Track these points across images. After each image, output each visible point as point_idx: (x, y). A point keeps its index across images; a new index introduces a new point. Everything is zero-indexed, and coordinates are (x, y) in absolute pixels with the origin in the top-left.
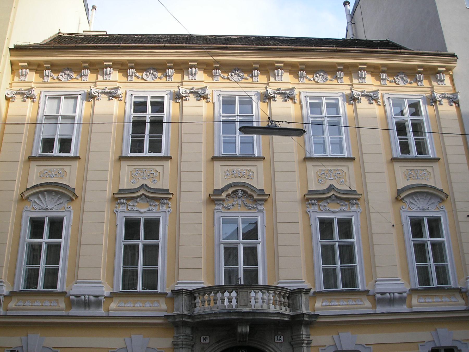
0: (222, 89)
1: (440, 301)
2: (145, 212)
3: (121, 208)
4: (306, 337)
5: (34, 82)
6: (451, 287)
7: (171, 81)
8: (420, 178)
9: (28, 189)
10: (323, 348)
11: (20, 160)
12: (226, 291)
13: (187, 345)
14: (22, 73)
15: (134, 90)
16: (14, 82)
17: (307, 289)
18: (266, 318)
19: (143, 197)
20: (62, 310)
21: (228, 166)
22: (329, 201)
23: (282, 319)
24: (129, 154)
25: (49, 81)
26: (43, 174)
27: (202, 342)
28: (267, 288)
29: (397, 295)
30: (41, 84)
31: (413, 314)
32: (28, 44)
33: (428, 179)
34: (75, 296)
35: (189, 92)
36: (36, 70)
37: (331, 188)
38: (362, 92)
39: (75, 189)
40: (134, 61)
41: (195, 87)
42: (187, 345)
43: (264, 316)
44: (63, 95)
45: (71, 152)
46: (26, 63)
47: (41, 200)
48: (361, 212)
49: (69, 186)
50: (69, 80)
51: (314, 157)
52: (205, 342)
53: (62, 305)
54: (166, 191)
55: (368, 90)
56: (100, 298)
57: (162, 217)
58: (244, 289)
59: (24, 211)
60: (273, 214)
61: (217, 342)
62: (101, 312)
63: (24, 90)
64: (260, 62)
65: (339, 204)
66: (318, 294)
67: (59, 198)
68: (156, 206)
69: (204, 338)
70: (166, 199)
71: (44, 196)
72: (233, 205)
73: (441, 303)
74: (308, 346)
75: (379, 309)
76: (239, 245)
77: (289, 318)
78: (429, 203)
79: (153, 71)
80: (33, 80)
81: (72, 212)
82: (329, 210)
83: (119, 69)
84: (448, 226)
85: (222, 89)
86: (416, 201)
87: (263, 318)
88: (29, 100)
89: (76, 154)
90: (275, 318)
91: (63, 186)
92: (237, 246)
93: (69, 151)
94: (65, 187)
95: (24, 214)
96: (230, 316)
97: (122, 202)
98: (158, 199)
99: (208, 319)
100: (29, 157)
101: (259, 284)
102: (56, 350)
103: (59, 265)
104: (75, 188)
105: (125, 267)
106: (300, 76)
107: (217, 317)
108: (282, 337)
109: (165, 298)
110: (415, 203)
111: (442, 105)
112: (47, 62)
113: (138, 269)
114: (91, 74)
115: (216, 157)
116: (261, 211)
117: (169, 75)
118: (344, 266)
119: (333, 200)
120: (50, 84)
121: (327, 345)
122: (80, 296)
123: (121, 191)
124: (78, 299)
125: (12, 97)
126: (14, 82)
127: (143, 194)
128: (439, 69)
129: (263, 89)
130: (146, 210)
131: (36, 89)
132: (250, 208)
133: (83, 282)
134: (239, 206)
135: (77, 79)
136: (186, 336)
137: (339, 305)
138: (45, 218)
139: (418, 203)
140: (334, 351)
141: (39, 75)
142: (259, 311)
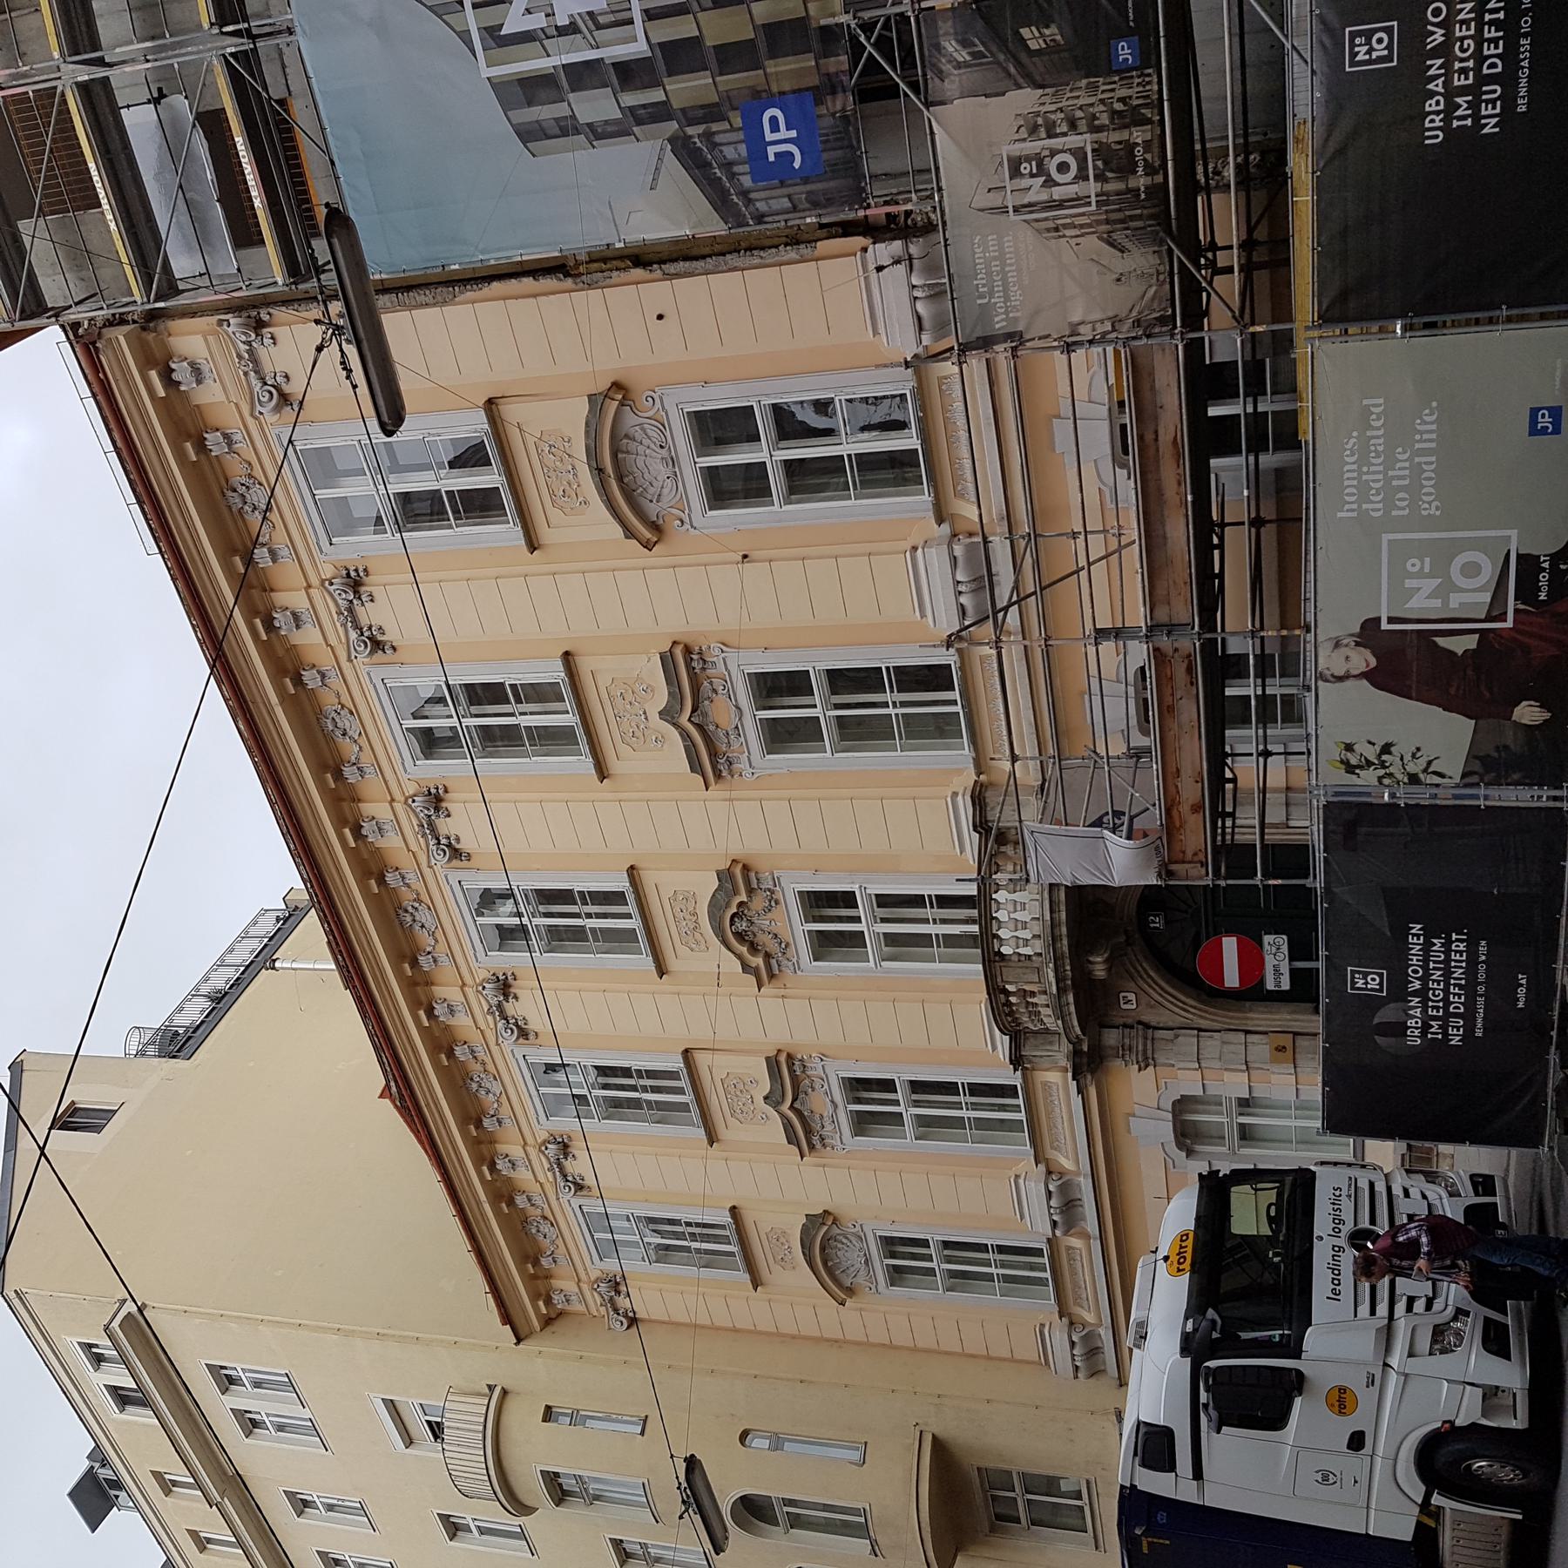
19: (797, 1105)
24: (584, 746)
27: (1134, 1007)
32: (489, 1295)
37: (668, 714)
44: (592, 1236)
46: (537, 1305)
52: (1134, 1002)
54: (667, 660)
76: (868, 891)
85: (312, 540)
92: (881, 936)
96: (1070, 1014)
99: (1065, 942)
101: (975, 893)
107: (1068, 1004)
119: (705, 715)
122: (961, 605)
124: (926, 324)
138: (700, 468)
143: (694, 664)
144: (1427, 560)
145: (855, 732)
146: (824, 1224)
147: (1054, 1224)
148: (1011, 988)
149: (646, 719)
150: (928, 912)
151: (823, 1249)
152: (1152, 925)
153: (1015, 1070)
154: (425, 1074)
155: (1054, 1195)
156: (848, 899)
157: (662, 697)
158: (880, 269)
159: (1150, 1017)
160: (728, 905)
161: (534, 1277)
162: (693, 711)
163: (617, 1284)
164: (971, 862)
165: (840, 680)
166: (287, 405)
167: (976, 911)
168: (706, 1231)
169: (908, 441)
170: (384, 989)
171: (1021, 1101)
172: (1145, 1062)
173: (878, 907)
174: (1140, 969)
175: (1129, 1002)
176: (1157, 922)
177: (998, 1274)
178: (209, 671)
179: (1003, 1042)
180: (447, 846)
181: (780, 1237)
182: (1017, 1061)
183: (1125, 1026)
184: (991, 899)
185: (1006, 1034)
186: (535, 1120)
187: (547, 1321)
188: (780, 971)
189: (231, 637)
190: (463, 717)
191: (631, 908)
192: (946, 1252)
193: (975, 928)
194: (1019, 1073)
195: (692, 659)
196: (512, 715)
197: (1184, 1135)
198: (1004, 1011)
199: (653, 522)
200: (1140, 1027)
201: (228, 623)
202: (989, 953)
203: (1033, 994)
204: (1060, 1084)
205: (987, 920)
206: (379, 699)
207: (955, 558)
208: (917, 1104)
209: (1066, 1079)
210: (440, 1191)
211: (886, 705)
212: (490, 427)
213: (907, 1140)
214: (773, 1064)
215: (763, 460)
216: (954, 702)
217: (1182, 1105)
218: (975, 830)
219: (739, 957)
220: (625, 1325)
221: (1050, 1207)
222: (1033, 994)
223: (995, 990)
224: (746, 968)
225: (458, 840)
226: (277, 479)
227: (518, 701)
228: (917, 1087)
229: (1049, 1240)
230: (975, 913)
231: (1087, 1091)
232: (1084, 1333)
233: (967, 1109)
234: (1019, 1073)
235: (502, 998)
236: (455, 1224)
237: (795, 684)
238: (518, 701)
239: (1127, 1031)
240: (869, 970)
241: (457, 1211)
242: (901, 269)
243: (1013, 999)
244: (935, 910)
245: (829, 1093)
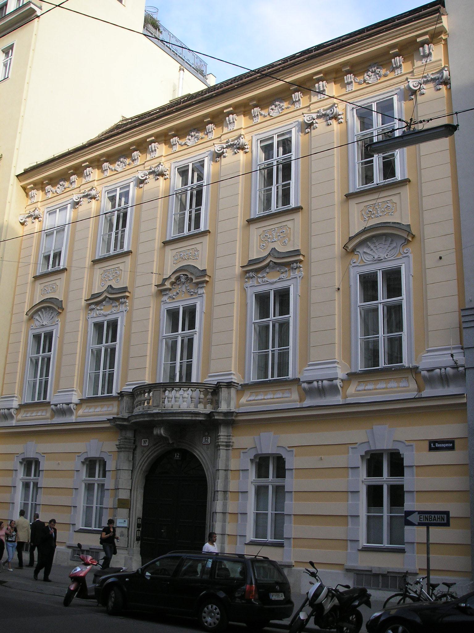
0: (178, 160)
1: (383, 387)
2: (108, 314)
3: (251, 283)
4: (227, 438)
5: (243, 127)
6: (403, 366)
7: (299, 108)
8: (381, 214)
9: (351, 239)
10: (245, 451)
11: (238, 227)
12: (189, 389)
13: (125, 448)
14: (229, 120)
15: (109, 185)
16: (312, 104)
17: (228, 382)
18: (174, 418)
19: (107, 299)
20: (295, 401)
21: (44, 284)
22: (267, 270)
23: (194, 418)
24: (262, 214)
25: (259, 121)
26: (44, 291)
28: (179, 385)
29: (325, 382)
30: (45, 201)
31: (353, 406)
33: (393, 213)
34: (307, 383)
35: (147, 173)
36: (244, 112)
38: (318, 112)
39: (410, 226)
40: (135, 142)
41: (152, 166)
42: (125, 448)
43: (172, 416)
44: (57, 208)
45: (396, 176)
47: (41, 317)
48: (302, 278)
49: (58, 299)
50: (281, 113)
51: (257, 218)
53: (295, 396)
54: (297, 253)
55: (325, 107)
56: (334, 381)
57: (120, 317)
58: (156, 388)
59: (351, 266)
60: (306, 279)
61: (154, 445)
62: (338, 400)
63: (88, 191)
64: (209, 114)
65: (279, 271)
66: (246, 387)
67: (52, 313)
68: (116, 306)
69: (144, 441)
70: (296, 262)
71: (42, 313)
72: (178, 294)
73: (399, 389)
74: (227, 448)
75: (308, 403)
77: (204, 417)
78: (390, 248)
79: (123, 159)
80: (243, 127)
81: (411, 256)
82: (267, 281)
83: (335, 79)
84: (298, 297)
85: (178, 160)
86: (374, 252)
87: (171, 418)
88: (241, 152)
89: (298, 205)
90: (185, 418)
91: (391, 225)
93: (394, 175)
94: (396, 226)
95: (90, 320)
96: (144, 417)
97: (251, 275)
98: (117, 299)
100: (346, 194)
101: (192, 382)
102: (411, 443)
103: (289, 346)
104: (409, 225)
105: (281, 350)
106: (253, 115)
108: (209, 438)
109: (118, 401)
110: (370, 252)
111: (424, 94)
112: (69, 168)
113: (268, 354)
114: (79, 178)
115: (351, 193)
116: (201, 295)
117: (254, 115)
118: (283, 349)
119: (273, 268)
120: (51, 199)
121: (249, 447)
122: (313, 382)
123: (252, 262)
125: (25, 222)
126: (312, 104)
127: (106, 297)
128: (419, 40)
129: (301, 116)
130: (109, 312)
131: (165, 163)
132: (192, 293)
133: (332, 362)
134: (183, 293)
135: (68, 187)
136: (126, 439)
137: (264, 399)
139: (374, 252)
140: (256, 454)
141: (248, 116)
142: (167, 412)
143: (295, 265)
144: (36, 552)
145: (263, 331)
146: (58, 308)
147: (56, 405)
148: (151, 394)
149: (273, 242)
150: (185, 360)
151: (49, 307)
152: (176, 454)
153: (118, 393)
154: (126, 139)
155: (330, 383)
156: (192, 326)
157: (281, 249)
158: (452, 355)
159: (138, 451)
160: (192, 274)
161: (42, 183)
162: (275, 263)
163: (38, 218)
164: (205, 380)
165: (284, 327)
166: (412, 93)
167: (185, 381)
168: (119, 241)
169: (382, 363)
170: (153, 126)
171: (106, 395)
172: (120, 448)
173: (188, 339)
174: (158, 448)
175: (145, 443)
176: (177, 456)
177: (37, 380)
178: (252, 70)
179: (129, 389)
180: (223, 152)
181: (54, 291)
182: (121, 395)
183: (135, 440)
184: (189, 388)
185: (133, 390)
186: (106, 185)
187: (24, 188)
188: (113, 307)
189: (273, 80)
190: (377, 131)
191: (193, 231)
192: (46, 359)
193: (177, 380)
194: (117, 395)
195: (297, 263)
196: (277, 183)
197: (90, 461)
198: (142, 390)
199: (355, 249)
200: (134, 447)
201: (278, 79)
202: (166, 385)
203: (148, 403)
204: (112, 412)
205: (180, 385)
206: (284, 126)
207: (333, 380)
208: (106, 350)
209: (113, 414)
210: (79, 144)
211: (273, 347)
212: (399, 181)
213: (31, 353)
214: (125, 289)
215: (270, 317)
216: (272, 376)
217: (103, 463)
218: (218, 382)
219: (170, 277)
220: (21, 221)
221: (63, 404)
222: (148, 403)
223: (151, 387)
224: (165, 280)
225: (225, 157)
226: (341, 100)
227: (283, 186)
228: (113, 350)
229: (49, 402)
230: (184, 380)
231: (108, 423)
232: (13, 414)
233: (103, 372)
234: (117, 395)
235: (157, 173)
236: (64, 150)
237: (284, 308)
238: (283, 186)
239: (133, 441)
240: (163, 334)
241: (85, 145)
242: (452, 363)
243: (147, 394)
244: (278, 351)
245: (112, 313)
